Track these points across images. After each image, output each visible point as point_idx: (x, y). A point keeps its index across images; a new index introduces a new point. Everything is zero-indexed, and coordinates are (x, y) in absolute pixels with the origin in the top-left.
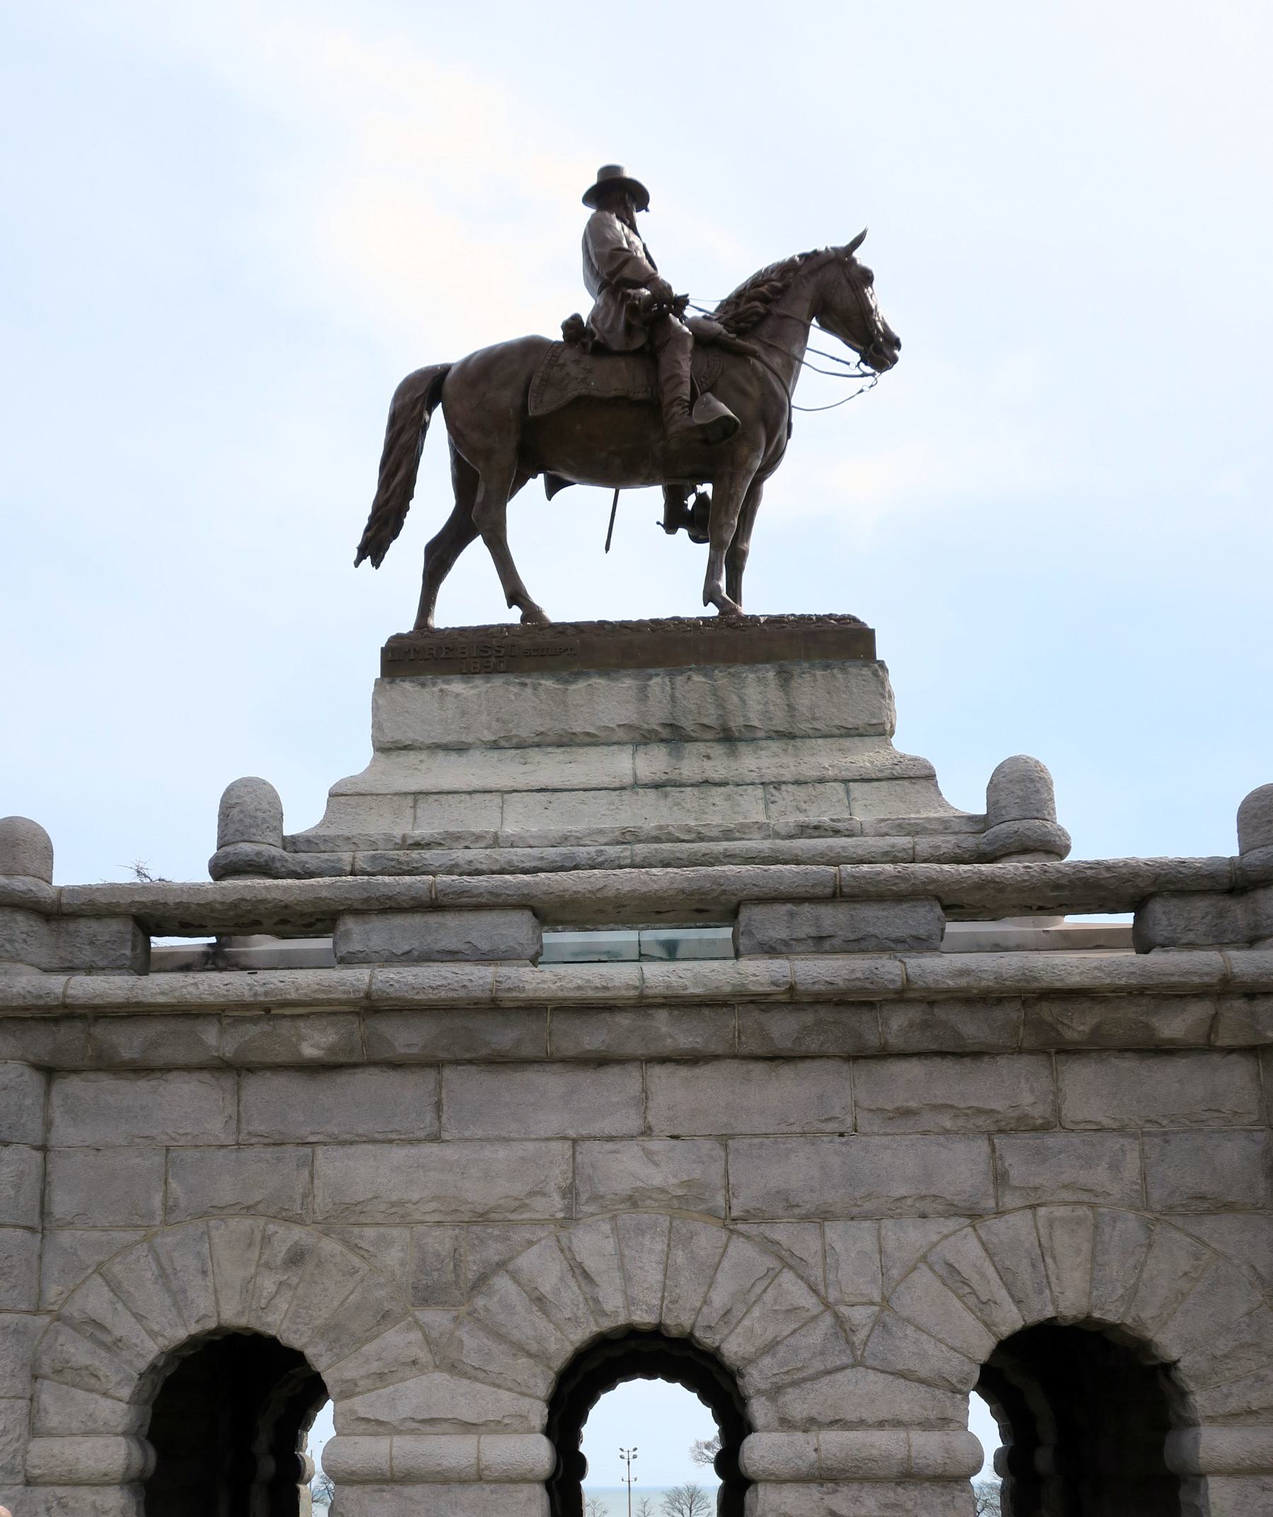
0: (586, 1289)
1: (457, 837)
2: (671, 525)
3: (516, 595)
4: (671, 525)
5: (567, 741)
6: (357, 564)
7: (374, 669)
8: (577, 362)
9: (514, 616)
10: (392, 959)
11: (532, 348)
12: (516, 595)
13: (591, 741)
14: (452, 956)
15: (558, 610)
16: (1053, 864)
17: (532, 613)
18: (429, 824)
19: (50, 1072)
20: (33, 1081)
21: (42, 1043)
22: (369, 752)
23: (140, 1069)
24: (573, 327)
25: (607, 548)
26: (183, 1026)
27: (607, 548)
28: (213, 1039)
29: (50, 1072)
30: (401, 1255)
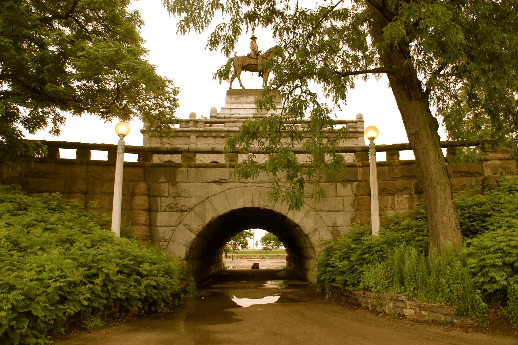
0: (104, 209)
1: (235, 114)
2: (259, 76)
3: (241, 86)
4: (259, 76)
5: (247, 103)
6: (220, 83)
7: (226, 94)
8: (48, 117)
9: (241, 88)
10: (231, 127)
11: (244, 57)
12: (241, 86)
13: (249, 103)
14: (236, 127)
15: (247, 87)
16: (149, 163)
17: (243, 88)
18: (232, 112)
19: (197, 137)
20: (196, 138)
21: (197, 134)
22: (225, 103)
23: (206, 137)
24: (249, 55)
25: (105, 123)
26: (210, 133)
27: (105, 123)
28: (214, 134)
29: (197, 137)
30: (246, 159)
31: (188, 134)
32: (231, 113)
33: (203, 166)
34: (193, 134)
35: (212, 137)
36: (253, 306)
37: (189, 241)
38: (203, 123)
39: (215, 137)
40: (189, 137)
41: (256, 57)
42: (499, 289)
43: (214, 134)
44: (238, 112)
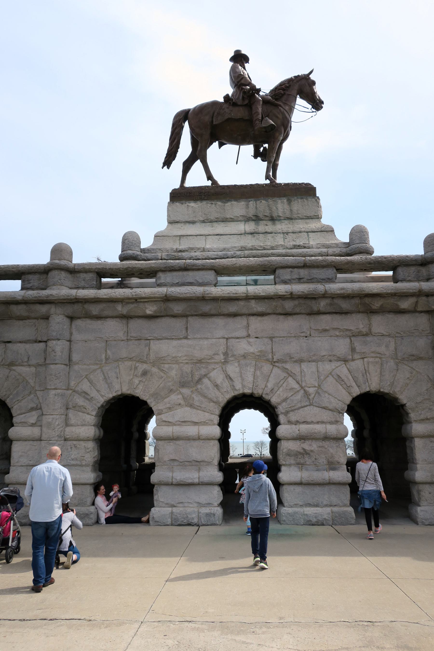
0: (230, 383)
1: (192, 249)
2: (255, 157)
3: (210, 177)
4: (255, 157)
5: (225, 220)
9: (209, 183)
10: (173, 285)
12: (210, 177)
13: (232, 220)
15: (222, 181)
17: (214, 182)
18: (184, 245)
19: (72, 318)
21: (69, 310)
23: (98, 318)
26: (111, 305)
28: (120, 309)
29: (72, 318)
31: (43, 309)
32: (182, 247)
33: (240, 298)
34: (59, 310)
35: (116, 317)
36: (23, 561)
37: (187, 481)
38: (91, 275)
39: (127, 317)
40: (46, 318)
41: (246, 102)
42: (152, 467)
43: (120, 309)
44: (200, 243)
